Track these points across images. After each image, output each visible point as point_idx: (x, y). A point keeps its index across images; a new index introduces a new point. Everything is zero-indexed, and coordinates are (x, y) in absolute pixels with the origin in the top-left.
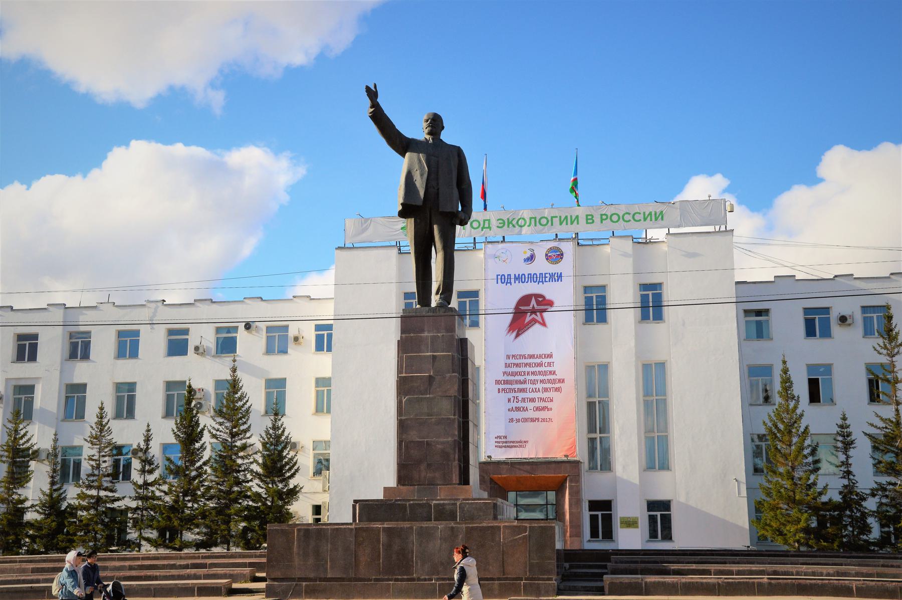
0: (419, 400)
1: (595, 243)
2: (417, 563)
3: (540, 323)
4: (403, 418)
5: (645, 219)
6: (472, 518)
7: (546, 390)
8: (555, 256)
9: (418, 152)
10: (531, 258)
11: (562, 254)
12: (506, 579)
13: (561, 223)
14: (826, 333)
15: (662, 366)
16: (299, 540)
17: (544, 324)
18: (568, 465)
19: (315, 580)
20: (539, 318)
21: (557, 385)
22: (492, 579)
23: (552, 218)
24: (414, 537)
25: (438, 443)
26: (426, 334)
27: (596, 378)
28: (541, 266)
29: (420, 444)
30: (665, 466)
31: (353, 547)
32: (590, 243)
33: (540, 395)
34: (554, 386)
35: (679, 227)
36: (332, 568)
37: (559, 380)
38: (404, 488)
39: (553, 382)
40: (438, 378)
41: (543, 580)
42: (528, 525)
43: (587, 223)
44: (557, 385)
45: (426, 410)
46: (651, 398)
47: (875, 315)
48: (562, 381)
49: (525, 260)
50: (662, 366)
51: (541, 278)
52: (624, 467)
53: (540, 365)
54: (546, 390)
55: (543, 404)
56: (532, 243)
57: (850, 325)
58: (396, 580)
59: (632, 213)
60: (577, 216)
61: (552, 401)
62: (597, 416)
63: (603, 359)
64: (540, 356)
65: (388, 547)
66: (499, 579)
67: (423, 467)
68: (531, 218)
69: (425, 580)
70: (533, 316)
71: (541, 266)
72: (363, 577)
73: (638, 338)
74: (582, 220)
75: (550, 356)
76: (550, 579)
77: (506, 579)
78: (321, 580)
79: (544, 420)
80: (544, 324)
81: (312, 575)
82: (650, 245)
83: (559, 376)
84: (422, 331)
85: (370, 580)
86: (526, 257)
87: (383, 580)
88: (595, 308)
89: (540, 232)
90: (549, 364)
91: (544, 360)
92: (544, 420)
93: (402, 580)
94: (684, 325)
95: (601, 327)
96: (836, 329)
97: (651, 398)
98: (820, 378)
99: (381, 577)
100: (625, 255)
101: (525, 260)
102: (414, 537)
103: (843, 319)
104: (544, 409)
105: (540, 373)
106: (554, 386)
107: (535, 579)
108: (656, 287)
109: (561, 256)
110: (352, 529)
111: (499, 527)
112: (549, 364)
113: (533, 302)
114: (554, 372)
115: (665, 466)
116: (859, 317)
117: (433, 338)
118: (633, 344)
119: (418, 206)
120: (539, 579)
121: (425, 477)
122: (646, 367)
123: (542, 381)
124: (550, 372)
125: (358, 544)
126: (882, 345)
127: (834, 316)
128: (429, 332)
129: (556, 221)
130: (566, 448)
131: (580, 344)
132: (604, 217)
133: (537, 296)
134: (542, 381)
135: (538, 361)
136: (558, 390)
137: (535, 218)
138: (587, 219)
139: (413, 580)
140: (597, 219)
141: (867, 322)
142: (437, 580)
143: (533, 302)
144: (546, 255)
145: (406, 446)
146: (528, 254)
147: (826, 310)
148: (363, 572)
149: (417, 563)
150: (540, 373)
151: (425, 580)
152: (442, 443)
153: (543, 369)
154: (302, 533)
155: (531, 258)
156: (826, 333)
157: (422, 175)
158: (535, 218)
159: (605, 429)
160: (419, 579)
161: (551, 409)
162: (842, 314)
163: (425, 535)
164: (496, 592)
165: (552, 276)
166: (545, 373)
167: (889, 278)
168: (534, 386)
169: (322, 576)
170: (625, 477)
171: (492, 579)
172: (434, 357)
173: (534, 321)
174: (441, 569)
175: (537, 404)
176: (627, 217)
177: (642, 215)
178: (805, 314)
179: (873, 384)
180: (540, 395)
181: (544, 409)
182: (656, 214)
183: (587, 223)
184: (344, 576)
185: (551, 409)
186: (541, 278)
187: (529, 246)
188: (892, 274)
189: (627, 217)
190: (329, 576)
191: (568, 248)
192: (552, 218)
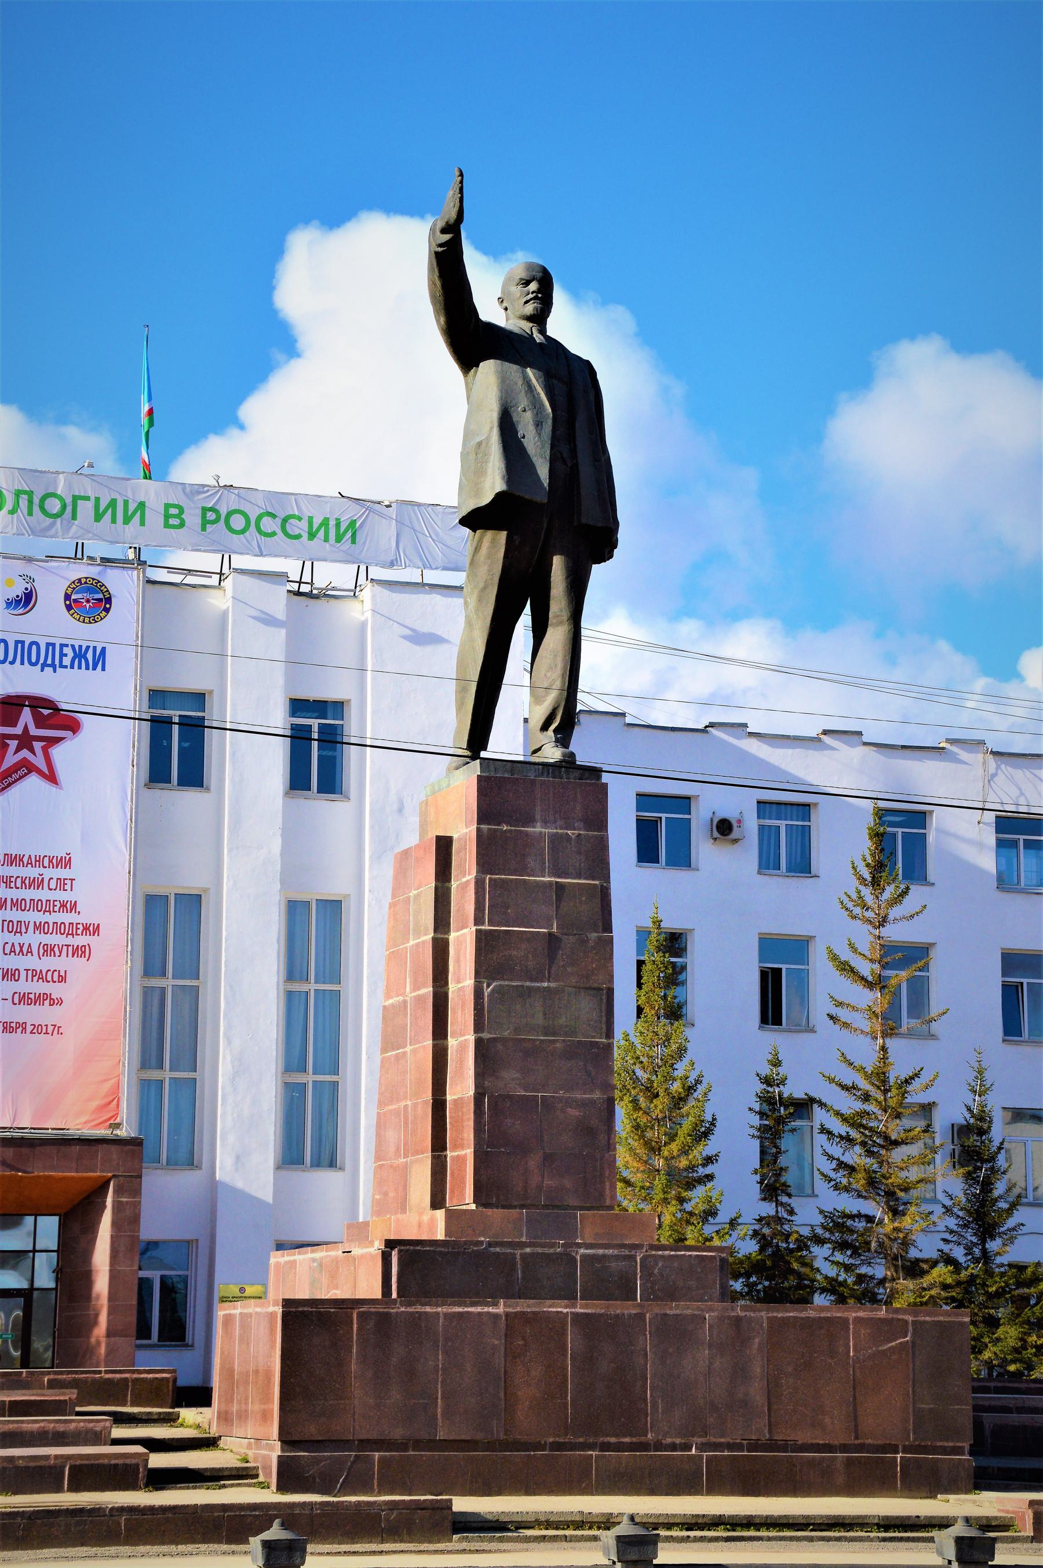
0: (525, 994)
1: (190, 580)
2: (654, 1404)
3: (40, 772)
4: (486, 1035)
5: (312, 535)
6: (671, 1294)
7: (48, 950)
8: (92, 600)
9: (524, 363)
10: (26, 600)
11: (109, 600)
12: (861, 1448)
13: (98, 517)
14: (682, 858)
15: (192, 904)
16: (363, 1341)
17: (51, 777)
18: (114, 1148)
19: (403, 1446)
20: (39, 761)
21: (80, 940)
22: (829, 1448)
23: (76, 498)
24: (647, 1342)
25: (569, 1103)
26: (538, 829)
27: (172, 928)
28: (52, 621)
29: (526, 1104)
30: (328, 1158)
31: (499, 1361)
32: (176, 578)
33: (32, 962)
34: (70, 941)
35: (392, 564)
36: (448, 1412)
37: (86, 928)
38: (496, 1215)
39: (71, 930)
40: (569, 941)
41: (945, 1451)
42: (910, 1318)
43: (167, 525)
44: (80, 940)
45: (539, 1020)
46: (303, 987)
47: (782, 824)
48: (91, 929)
49: (9, 604)
50: (192, 904)
51: (50, 656)
52: (238, 1158)
53: (37, 883)
54: (48, 950)
55: (38, 987)
56: (30, 560)
57: (735, 841)
58: (605, 1447)
59: (282, 515)
60: (142, 505)
61: (62, 979)
62: (169, 1032)
63: (190, 882)
64: (38, 861)
65: (587, 1361)
66: (844, 1448)
67: (533, 1162)
68: (18, 494)
69: (673, 1447)
70: (25, 753)
71: (52, 621)
72: (524, 1438)
73: (293, 835)
74: (154, 518)
75: (65, 862)
76: (958, 1451)
77: (861, 1448)
78: (418, 1444)
79: (37, 1029)
80: (51, 777)
81: (398, 1433)
82: (322, 602)
83: (84, 918)
84: (530, 821)
85: (539, 1446)
86: (12, 595)
87: (573, 1447)
88: (178, 744)
89: (43, 532)
90: (61, 884)
91: (49, 873)
92: (37, 1029)
93: (619, 1447)
94: (400, 810)
95: (190, 796)
96: (704, 849)
97: (303, 987)
98: (784, 967)
99: (570, 1438)
100: (269, 621)
101: (9, 604)
102: (647, 1342)
103: (724, 828)
104: (40, 999)
105: (36, 905)
106: (70, 941)
107: (925, 1450)
108: (328, 708)
109: (106, 602)
110: (496, 1316)
111: (846, 1320)
112: (61, 884)
113: (26, 716)
114: (73, 907)
115: (328, 1158)
116: (751, 824)
117: (555, 839)
118: (276, 846)
119: (530, 503)
120: (934, 1450)
121: (540, 1188)
122: (295, 910)
123: (38, 927)
124: (63, 905)
125: (513, 1355)
126: (854, 896)
127: (700, 817)
128: (545, 823)
129: (85, 509)
130: (95, 1104)
131: (145, 838)
132: (210, 516)
133: (37, 703)
134: (38, 927)
135: (32, 872)
136: (80, 951)
137: (30, 494)
138: (167, 516)
139: (644, 1446)
140: (193, 519)
141: (768, 837)
142: (702, 1447)
143: (26, 716)
144: (67, 597)
145: (494, 1106)
146: (18, 589)
147: (684, 803)
148: (526, 1421)
149: (654, 1404)
150: (36, 905)
151: (673, 1447)
152: (583, 1104)
153: (43, 894)
154: (371, 1324)
155: (26, 600)
156: (682, 858)
157: (538, 424)
158: (30, 494)
159: (189, 1054)
160: (659, 1446)
161: (60, 1002)
162: (722, 814)
163: (676, 1334)
164: (840, 1480)
165: (80, 655)
166: (48, 907)
167: (816, 740)
168: (17, 939)
169: (424, 1435)
170: (239, 1184)
171: (829, 1448)
172: (560, 887)
173: (26, 768)
174: (711, 1420)
175: (24, 986)
176: (268, 524)
177: (304, 525)
178: (639, 809)
179: (771, 984)
180: (32, 962)
181: (40, 999)
182: (338, 525)
183: (167, 525)
184: (479, 1436)
185: (60, 1002)
186: (50, 656)
187: (20, 567)
188: (825, 732)
189: (268, 524)
190: (441, 1435)
191: (124, 586)
192: (76, 498)
